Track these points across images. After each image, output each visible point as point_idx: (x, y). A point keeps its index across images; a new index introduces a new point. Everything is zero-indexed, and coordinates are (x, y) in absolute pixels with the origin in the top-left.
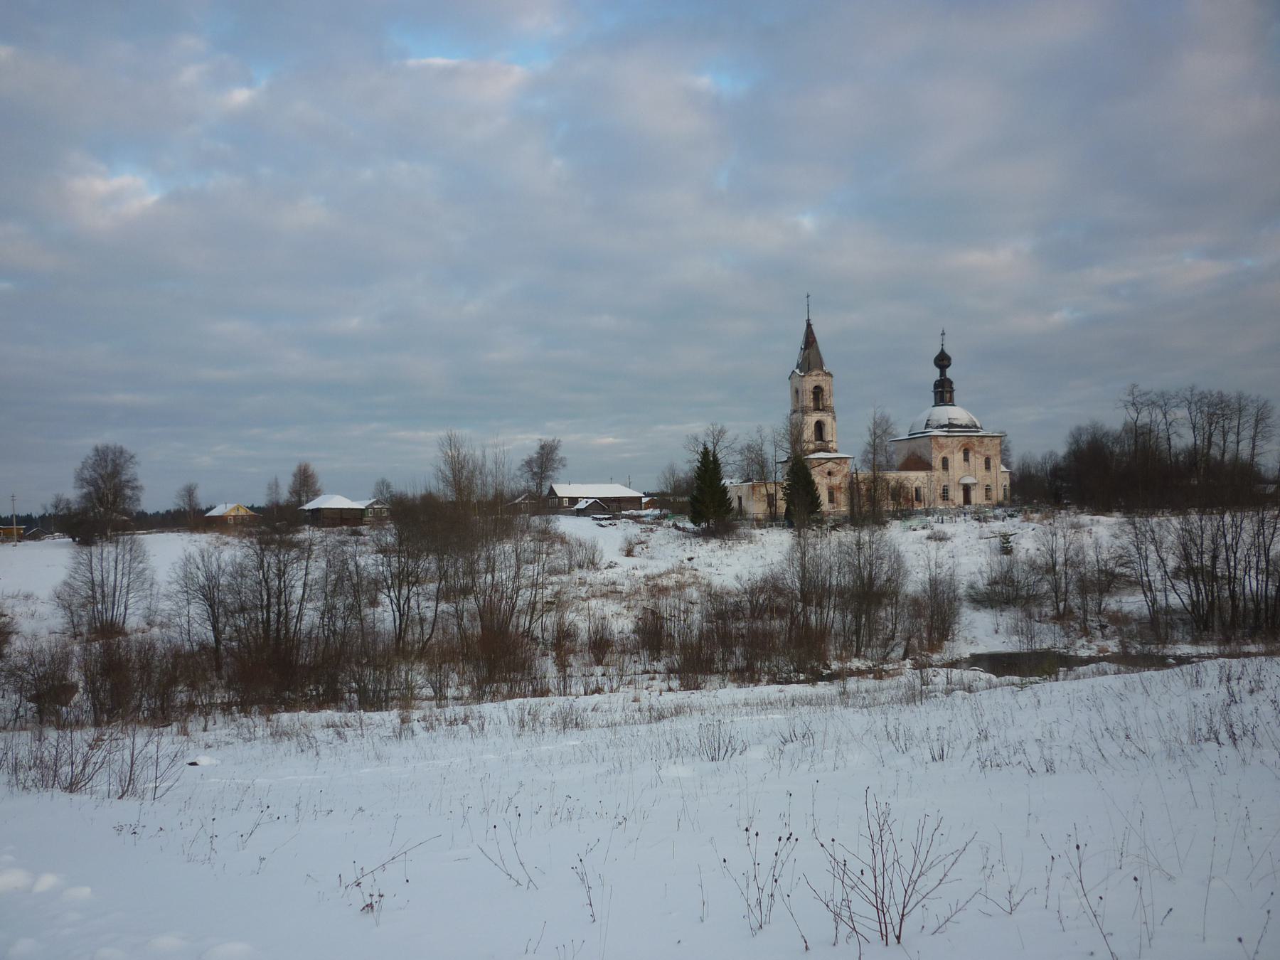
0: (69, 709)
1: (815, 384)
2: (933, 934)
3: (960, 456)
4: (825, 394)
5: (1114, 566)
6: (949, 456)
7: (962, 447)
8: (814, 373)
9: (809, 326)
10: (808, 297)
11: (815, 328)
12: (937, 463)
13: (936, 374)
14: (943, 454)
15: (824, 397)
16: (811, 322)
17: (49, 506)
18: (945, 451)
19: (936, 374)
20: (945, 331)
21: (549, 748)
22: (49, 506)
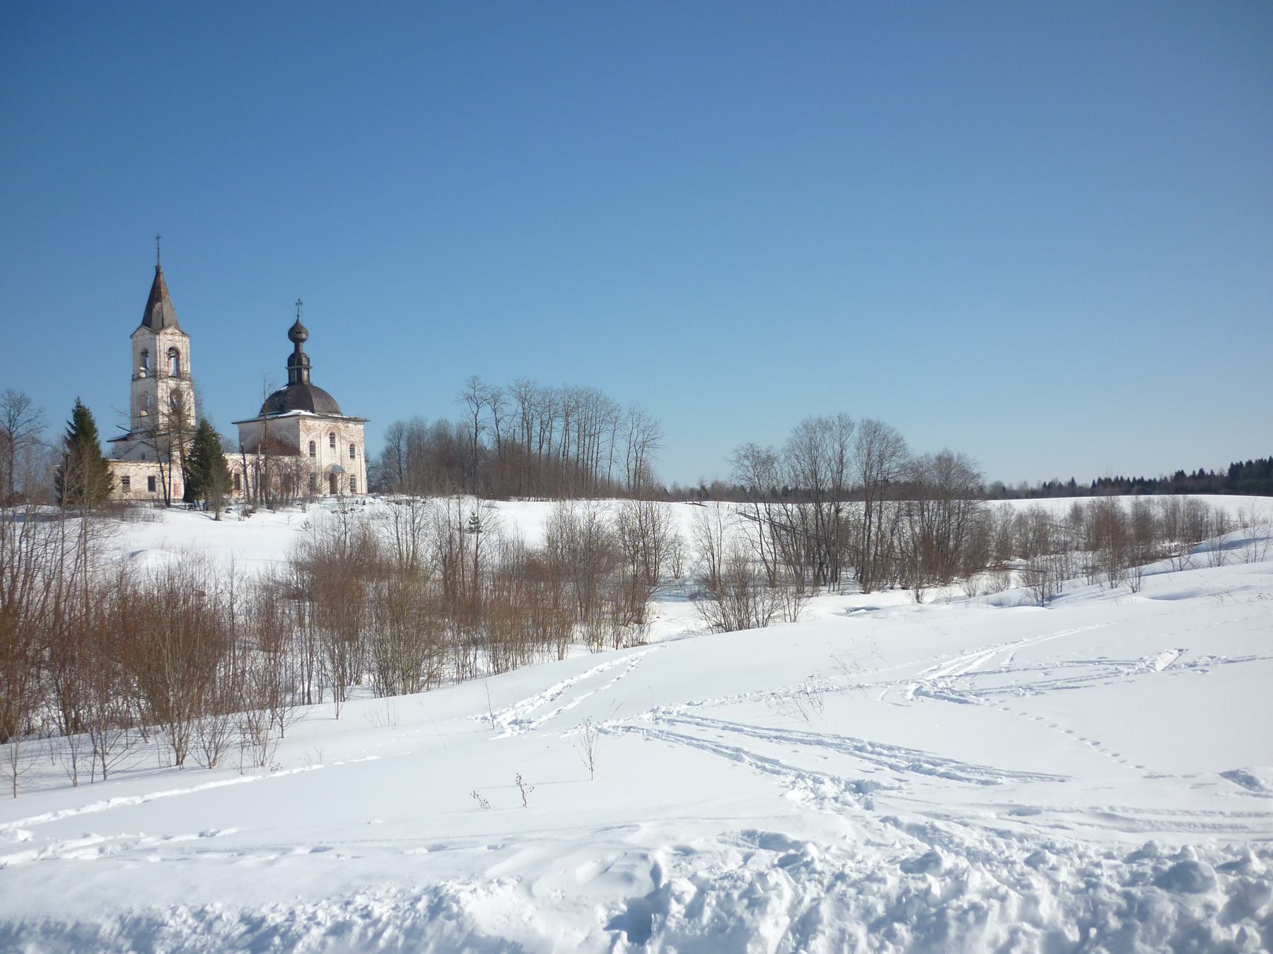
0: (798, 568)
1: (170, 345)
2: (914, 812)
3: (327, 440)
4: (181, 358)
5: (692, 561)
6: (315, 440)
7: (328, 430)
8: (169, 331)
9: (158, 273)
10: (158, 238)
11: (163, 278)
12: (304, 448)
13: (290, 348)
14: (310, 438)
15: (181, 362)
16: (161, 270)
17: (894, 434)
18: (313, 434)
19: (290, 348)
20: (302, 301)
21: (601, 667)
22: (894, 434)
